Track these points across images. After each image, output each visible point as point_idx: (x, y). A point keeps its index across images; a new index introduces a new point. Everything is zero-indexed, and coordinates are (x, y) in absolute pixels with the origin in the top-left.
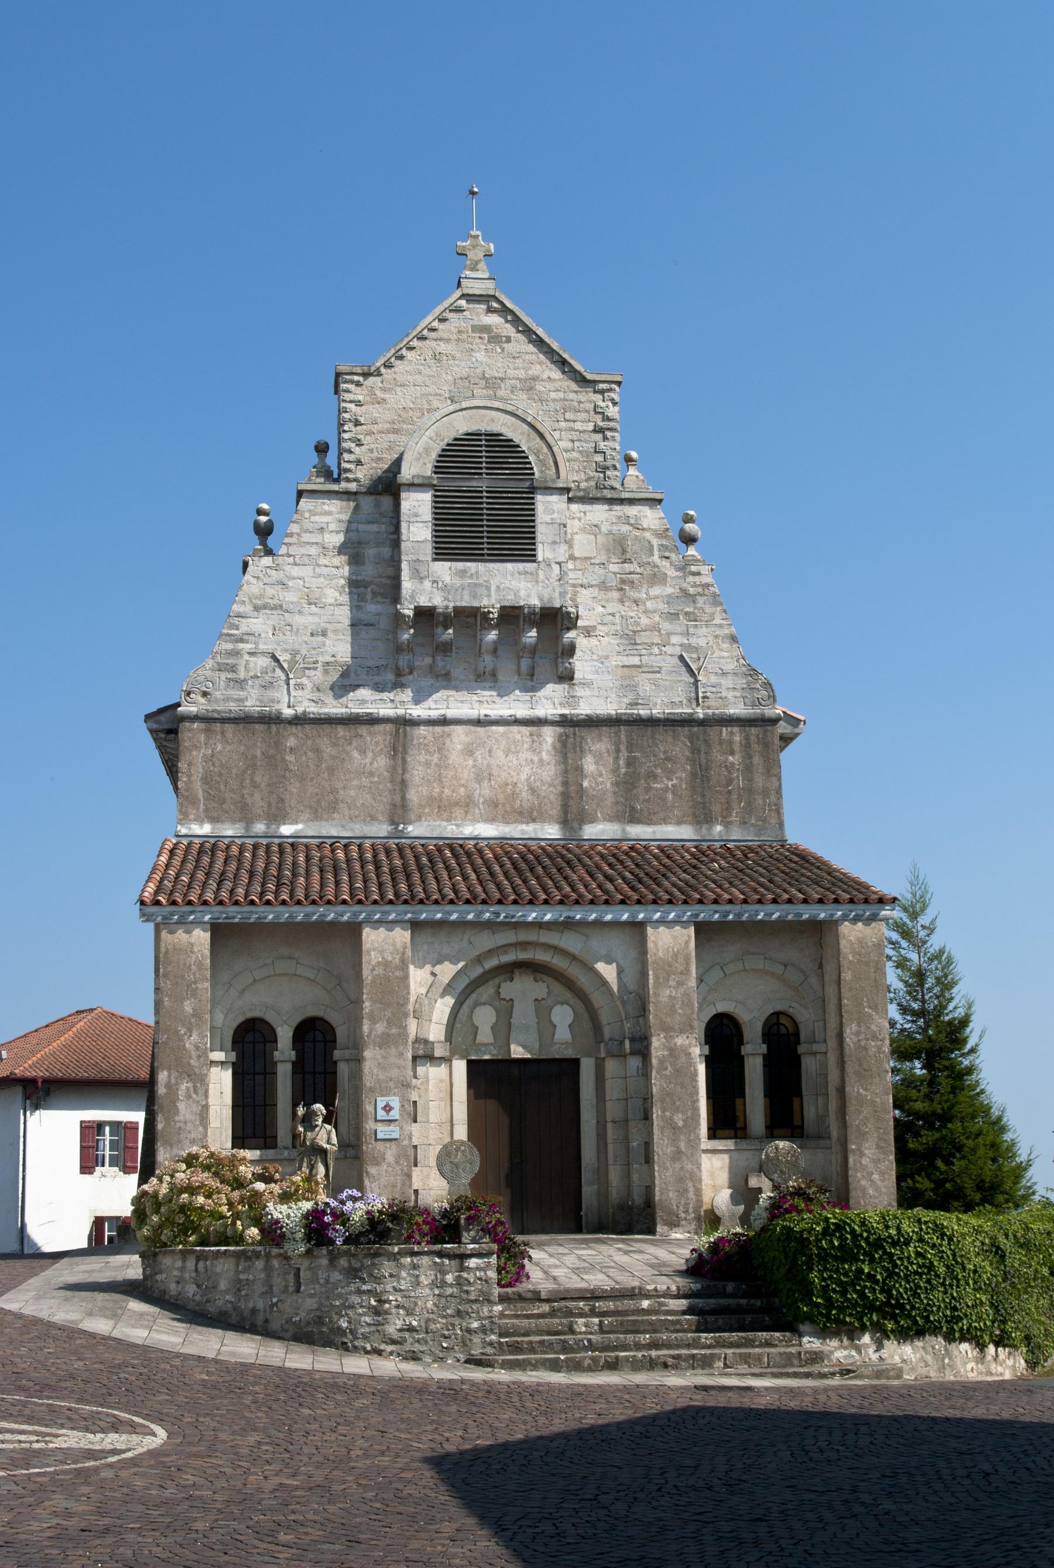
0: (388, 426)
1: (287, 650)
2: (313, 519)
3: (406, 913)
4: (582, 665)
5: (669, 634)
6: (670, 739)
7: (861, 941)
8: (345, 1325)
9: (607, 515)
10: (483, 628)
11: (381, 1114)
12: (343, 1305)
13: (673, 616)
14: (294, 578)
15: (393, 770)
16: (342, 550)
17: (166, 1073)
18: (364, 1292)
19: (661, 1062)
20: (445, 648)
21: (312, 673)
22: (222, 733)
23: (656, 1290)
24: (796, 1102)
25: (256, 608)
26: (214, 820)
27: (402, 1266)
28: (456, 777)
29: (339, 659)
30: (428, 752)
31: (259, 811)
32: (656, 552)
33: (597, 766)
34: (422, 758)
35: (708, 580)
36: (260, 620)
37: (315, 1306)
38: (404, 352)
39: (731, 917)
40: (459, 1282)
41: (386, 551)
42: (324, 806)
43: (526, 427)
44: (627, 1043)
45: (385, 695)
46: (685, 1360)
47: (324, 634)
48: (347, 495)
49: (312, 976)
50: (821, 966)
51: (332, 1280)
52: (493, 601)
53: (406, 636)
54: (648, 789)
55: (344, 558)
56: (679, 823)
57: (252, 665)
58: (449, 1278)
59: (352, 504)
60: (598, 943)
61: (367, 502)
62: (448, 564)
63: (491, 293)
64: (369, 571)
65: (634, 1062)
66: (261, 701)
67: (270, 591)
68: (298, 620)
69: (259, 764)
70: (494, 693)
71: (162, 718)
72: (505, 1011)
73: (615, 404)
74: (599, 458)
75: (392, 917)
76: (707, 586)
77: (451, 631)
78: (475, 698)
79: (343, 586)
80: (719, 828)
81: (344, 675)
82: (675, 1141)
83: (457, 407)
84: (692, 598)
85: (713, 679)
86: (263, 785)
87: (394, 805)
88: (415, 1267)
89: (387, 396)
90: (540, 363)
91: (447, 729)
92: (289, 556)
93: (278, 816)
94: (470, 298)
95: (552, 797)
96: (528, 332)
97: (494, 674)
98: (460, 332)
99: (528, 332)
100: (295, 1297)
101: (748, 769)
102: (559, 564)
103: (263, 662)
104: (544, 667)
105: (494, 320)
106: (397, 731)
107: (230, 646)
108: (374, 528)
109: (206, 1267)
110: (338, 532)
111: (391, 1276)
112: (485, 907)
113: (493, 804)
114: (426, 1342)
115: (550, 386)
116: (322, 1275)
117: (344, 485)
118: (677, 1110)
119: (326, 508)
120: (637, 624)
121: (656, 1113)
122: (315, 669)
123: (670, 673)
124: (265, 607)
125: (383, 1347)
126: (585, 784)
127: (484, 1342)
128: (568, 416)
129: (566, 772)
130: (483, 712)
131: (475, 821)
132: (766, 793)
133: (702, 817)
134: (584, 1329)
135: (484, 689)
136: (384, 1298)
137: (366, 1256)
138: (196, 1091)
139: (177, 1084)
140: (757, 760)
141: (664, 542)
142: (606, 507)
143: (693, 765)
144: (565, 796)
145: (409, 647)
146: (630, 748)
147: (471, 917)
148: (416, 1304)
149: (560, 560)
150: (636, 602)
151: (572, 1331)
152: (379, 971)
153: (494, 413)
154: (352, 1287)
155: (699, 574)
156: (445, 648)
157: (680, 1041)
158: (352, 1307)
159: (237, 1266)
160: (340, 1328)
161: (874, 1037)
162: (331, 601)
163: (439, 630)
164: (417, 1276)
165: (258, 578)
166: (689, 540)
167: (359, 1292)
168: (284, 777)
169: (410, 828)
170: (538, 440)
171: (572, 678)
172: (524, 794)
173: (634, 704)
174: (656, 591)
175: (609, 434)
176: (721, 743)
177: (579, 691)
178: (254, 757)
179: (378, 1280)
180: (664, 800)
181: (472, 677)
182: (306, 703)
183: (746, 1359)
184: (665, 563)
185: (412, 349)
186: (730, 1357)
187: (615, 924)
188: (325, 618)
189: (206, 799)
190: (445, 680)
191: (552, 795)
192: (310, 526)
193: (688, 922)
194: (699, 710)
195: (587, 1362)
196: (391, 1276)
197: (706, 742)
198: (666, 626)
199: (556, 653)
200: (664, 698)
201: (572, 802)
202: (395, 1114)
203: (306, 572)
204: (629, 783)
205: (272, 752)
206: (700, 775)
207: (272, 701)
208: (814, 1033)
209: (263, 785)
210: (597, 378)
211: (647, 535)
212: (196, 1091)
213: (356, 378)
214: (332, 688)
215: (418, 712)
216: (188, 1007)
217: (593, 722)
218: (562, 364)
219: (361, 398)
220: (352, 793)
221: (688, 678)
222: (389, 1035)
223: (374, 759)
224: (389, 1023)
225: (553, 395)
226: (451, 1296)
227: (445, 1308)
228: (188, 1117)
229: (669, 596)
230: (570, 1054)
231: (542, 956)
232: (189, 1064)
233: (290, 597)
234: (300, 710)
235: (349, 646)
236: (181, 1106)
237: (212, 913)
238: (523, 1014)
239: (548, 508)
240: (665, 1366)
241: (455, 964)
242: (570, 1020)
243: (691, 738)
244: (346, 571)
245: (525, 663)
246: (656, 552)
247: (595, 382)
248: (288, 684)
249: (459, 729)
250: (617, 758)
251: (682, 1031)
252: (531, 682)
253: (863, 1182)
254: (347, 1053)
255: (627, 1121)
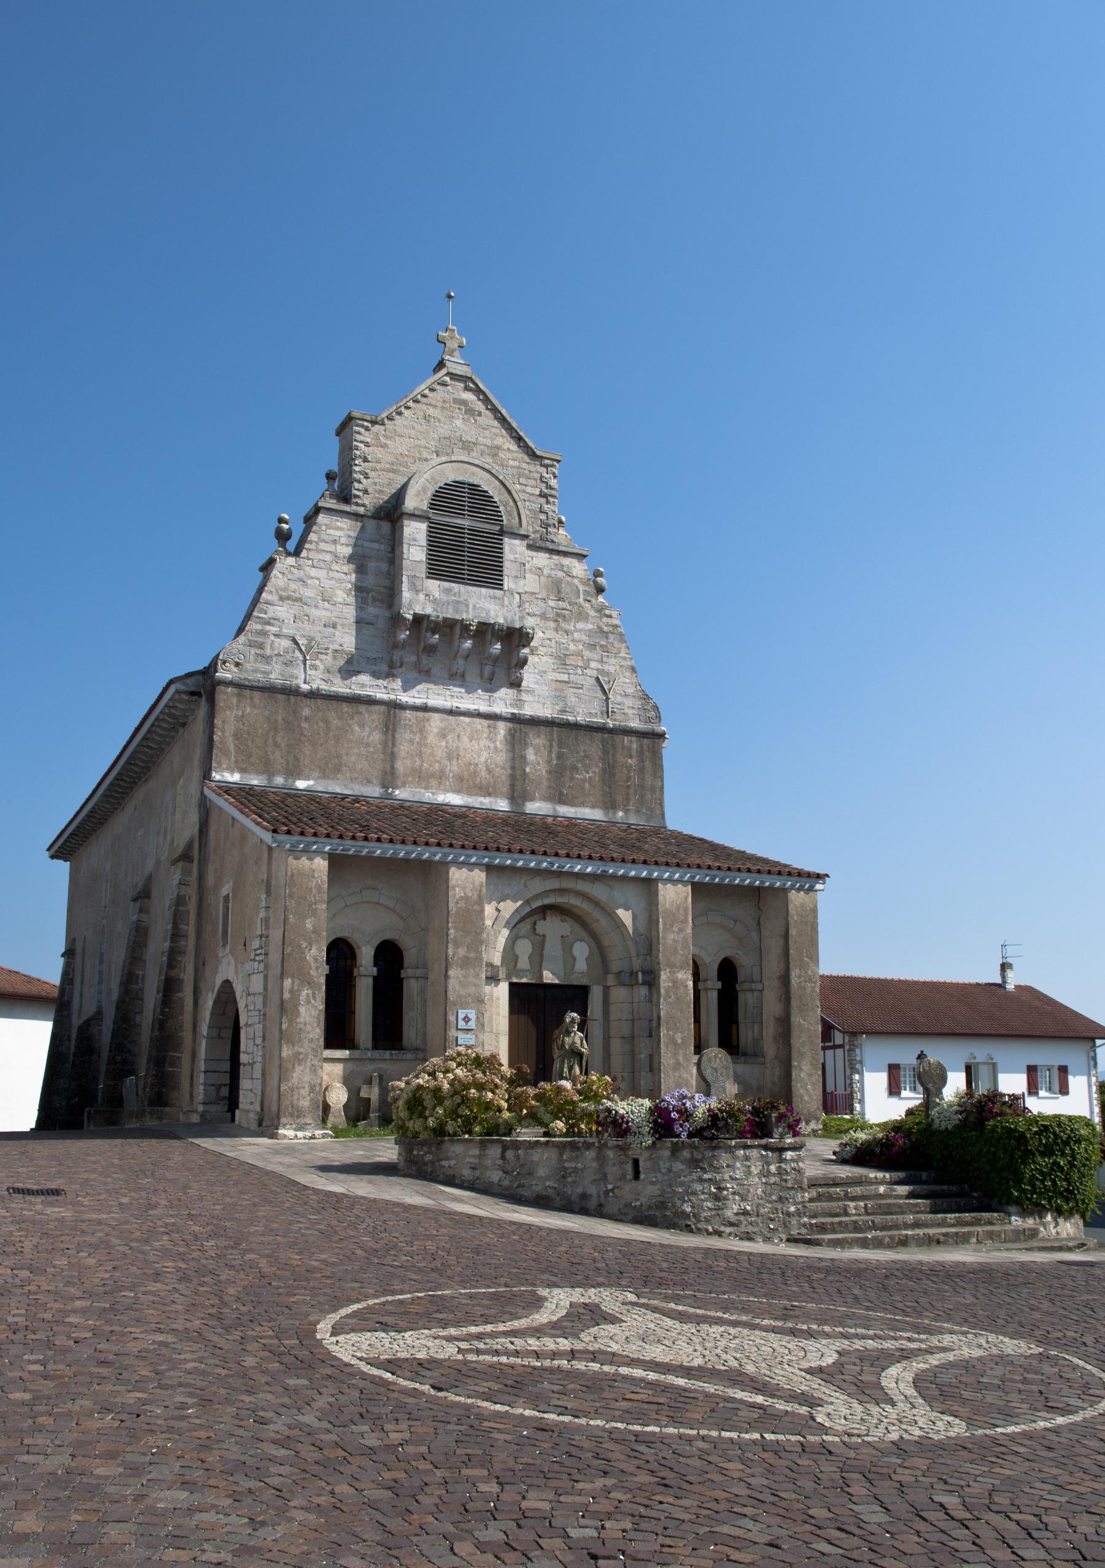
0: (388, 466)
1: (304, 636)
2: (329, 531)
3: (484, 858)
4: (529, 676)
5: (589, 660)
6: (588, 741)
7: (802, 905)
8: (689, 1209)
9: (547, 562)
10: (461, 637)
11: (462, 1024)
12: (686, 1192)
13: (592, 647)
14: (312, 578)
15: (385, 744)
16: (351, 559)
17: (290, 980)
18: (705, 1180)
19: (667, 991)
20: (431, 650)
21: (324, 657)
22: (251, 698)
23: (876, 1178)
24: (734, 1027)
25: (282, 599)
26: (242, 771)
27: (736, 1158)
28: (432, 754)
29: (345, 648)
30: (412, 732)
31: (279, 767)
32: (582, 596)
33: (536, 756)
34: (407, 736)
35: (616, 622)
36: (284, 608)
37: (657, 1193)
38: (403, 409)
39: (717, 880)
40: (781, 1172)
41: (384, 566)
42: (331, 768)
43: (498, 483)
44: (640, 974)
45: (380, 682)
46: (952, 1237)
47: (334, 626)
48: (356, 516)
49: (391, 905)
50: (759, 923)
51: (674, 1169)
52: (471, 617)
53: (403, 636)
54: (572, 779)
55: (352, 567)
56: (593, 807)
57: (276, 645)
58: (773, 1168)
59: (359, 524)
60: (620, 893)
61: (371, 524)
62: (438, 582)
63: (469, 375)
64: (370, 581)
65: (643, 991)
66: (283, 676)
67: (293, 586)
68: (315, 613)
69: (280, 727)
70: (463, 690)
71: (190, 681)
72: (539, 944)
73: (555, 477)
74: (543, 517)
75: (473, 860)
76: (616, 626)
77: (437, 636)
78: (448, 692)
79: (350, 590)
80: (621, 814)
81: (349, 662)
82: (675, 1054)
83: (444, 459)
84: (606, 635)
85: (619, 699)
86: (283, 745)
87: (385, 772)
88: (747, 1158)
89: (388, 442)
90: (502, 436)
91: (427, 715)
92: (309, 559)
93: (294, 772)
94: (453, 376)
95: (503, 778)
96: (495, 410)
97: (463, 676)
98: (444, 401)
99: (495, 410)
100: (634, 1184)
101: (641, 771)
102: (519, 594)
103: (286, 643)
104: (500, 674)
105: (469, 396)
106: (389, 712)
107: (259, 627)
108: (376, 546)
109: (518, 1157)
110: (347, 545)
111: (728, 1166)
112: (544, 857)
113: (460, 779)
114: (757, 1224)
115: (509, 455)
116: (664, 1165)
117: (354, 508)
118: (677, 1030)
119: (339, 524)
120: (567, 649)
121: (663, 1031)
122: (327, 654)
123: (589, 690)
124: (289, 598)
125: (722, 1229)
126: (528, 770)
127: (799, 1223)
128: (522, 480)
129: (513, 759)
130: (455, 705)
131: (446, 791)
132: (653, 790)
133: (610, 805)
134: (854, 1212)
135: (455, 686)
136: (723, 1185)
137: (707, 1148)
138: (314, 998)
139: (299, 990)
140: (648, 764)
141: (587, 589)
142: (547, 555)
143: (604, 763)
144: (513, 777)
145: (404, 645)
146: (560, 746)
147: (532, 864)
148: (749, 1191)
149: (520, 591)
150: (567, 632)
151: (846, 1214)
152: (462, 904)
153: (475, 469)
154: (694, 1176)
155: (610, 616)
156: (431, 650)
157: (680, 975)
158: (694, 1193)
159: (561, 1155)
160: (683, 1212)
161: (810, 980)
162: (340, 600)
163: (429, 634)
164: (749, 1167)
165: (283, 574)
166: (600, 590)
167: (701, 1180)
168: (299, 740)
169: (397, 792)
170: (506, 495)
171: (520, 686)
172: (483, 773)
173: (563, 711)
174: (580, 625)
175: (551, 500)
176: (623, 748)
177: (525, 697)
178: (276, 721)
179: (717, 1170)
180: (583, 788)
181: (446, 676)
182: (319, 682)
183: (991, 1235)
184: (587, 605)
185: (408, 408)
186: (981, 1233)
187: (636, 879)
188: (335, 614)
189: (236, 752)
190: (425, 675)
191: (503, 775)
192: (326, 538)
193: (687, 881)
194: (608, 721)
195: (887, 1240)
196: (728, 1166)
197: (613, 746)
198: (587, 654)
199: (509, 664)
200: (586, 711)
201: (517, 783)
202: (472, 1024)
203: (322, 574)
204: (559, 772)
205: (290, 718)
206: (609, 772)
207: (292, 676)
208: (752, 974)
209: (283, 745)
210: (544, 455)
211: (576, 581)
212: (314, 998)
213: (366, 424)
214: (340, 671)
215: (405, 698)
216: (309, 924)
217: (535, 722)
218: (519, 439)
219: (369, 440)
220: (353, 759)
221: (600, 695)
222: (467, 958)
223: (371, 733)
224: (469, 948)
225: (511, 463)
226: (774, 1184)
227: (770, 1195)
228: (308, 1019)
229: (590, 631)
230: (584, 981)
231: (574, 901)
232: (309, 973)
233: (308, 593)
234: (315, 686)
235: (353, 639)
236: (302, 1010)
237: (331, 844)
238: (553, 947)
239: (513, 550)
240: (938, 1242)
241: (515, 901)
242: (587, 953)
243: (603, 741)
244: (353, 577)
245: (488, 670)
246: (582, 596)
247: (542, 458)
248: (305, 664)
249: (436, 716)
250: (550, 752)
251: (681, 968)
252: (490, 685)
253: (802, 1091)
254: (419, 972)
255: (633, 1037)
